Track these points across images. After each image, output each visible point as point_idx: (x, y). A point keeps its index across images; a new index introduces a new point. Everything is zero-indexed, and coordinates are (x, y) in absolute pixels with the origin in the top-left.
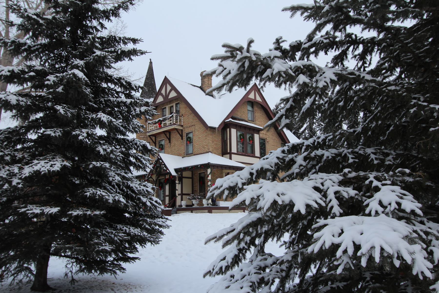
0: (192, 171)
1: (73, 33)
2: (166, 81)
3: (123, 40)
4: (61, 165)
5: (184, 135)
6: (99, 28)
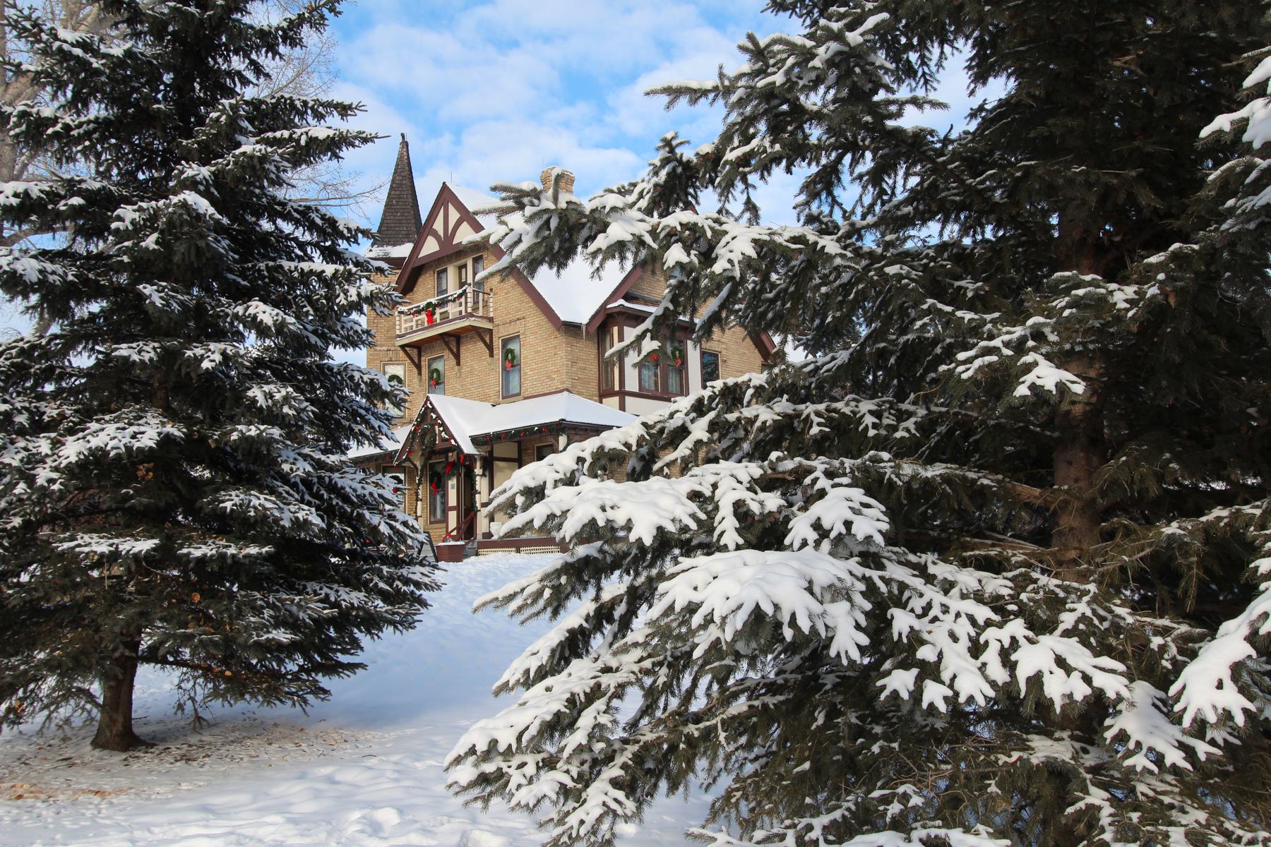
0: (519, 443)
1: (181, 87)
2: (445, 196)
3: (312, 108)
4: (159, 434)
5: (498, 344)
6: (250, 75)
